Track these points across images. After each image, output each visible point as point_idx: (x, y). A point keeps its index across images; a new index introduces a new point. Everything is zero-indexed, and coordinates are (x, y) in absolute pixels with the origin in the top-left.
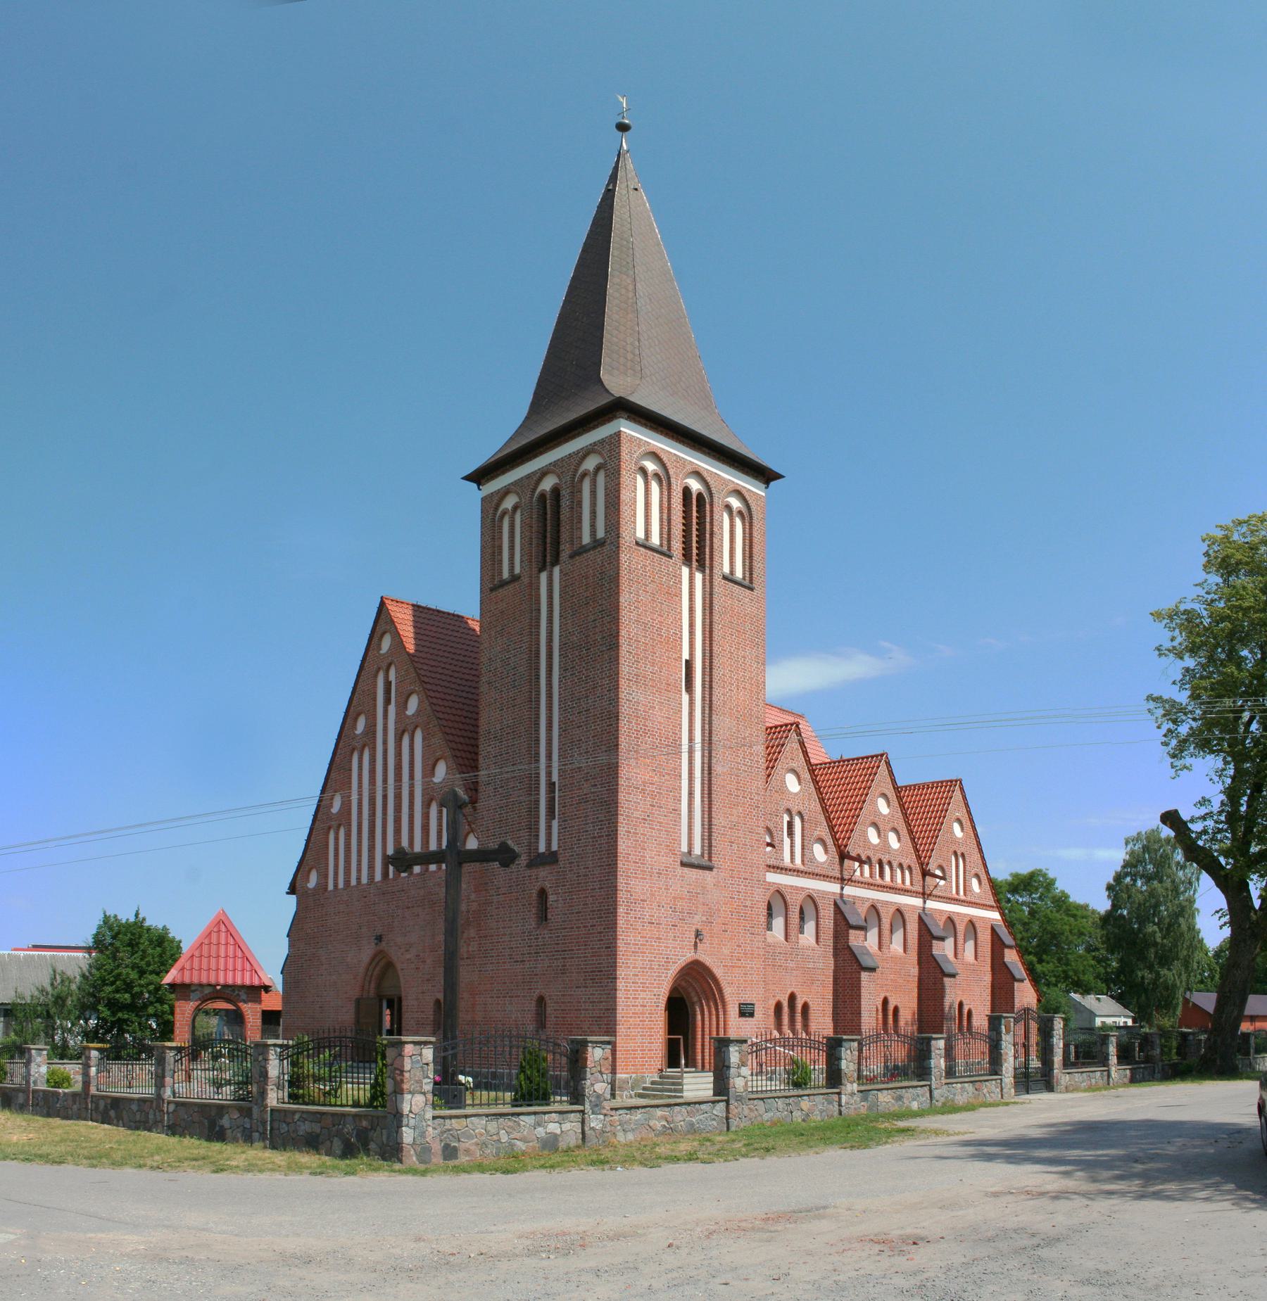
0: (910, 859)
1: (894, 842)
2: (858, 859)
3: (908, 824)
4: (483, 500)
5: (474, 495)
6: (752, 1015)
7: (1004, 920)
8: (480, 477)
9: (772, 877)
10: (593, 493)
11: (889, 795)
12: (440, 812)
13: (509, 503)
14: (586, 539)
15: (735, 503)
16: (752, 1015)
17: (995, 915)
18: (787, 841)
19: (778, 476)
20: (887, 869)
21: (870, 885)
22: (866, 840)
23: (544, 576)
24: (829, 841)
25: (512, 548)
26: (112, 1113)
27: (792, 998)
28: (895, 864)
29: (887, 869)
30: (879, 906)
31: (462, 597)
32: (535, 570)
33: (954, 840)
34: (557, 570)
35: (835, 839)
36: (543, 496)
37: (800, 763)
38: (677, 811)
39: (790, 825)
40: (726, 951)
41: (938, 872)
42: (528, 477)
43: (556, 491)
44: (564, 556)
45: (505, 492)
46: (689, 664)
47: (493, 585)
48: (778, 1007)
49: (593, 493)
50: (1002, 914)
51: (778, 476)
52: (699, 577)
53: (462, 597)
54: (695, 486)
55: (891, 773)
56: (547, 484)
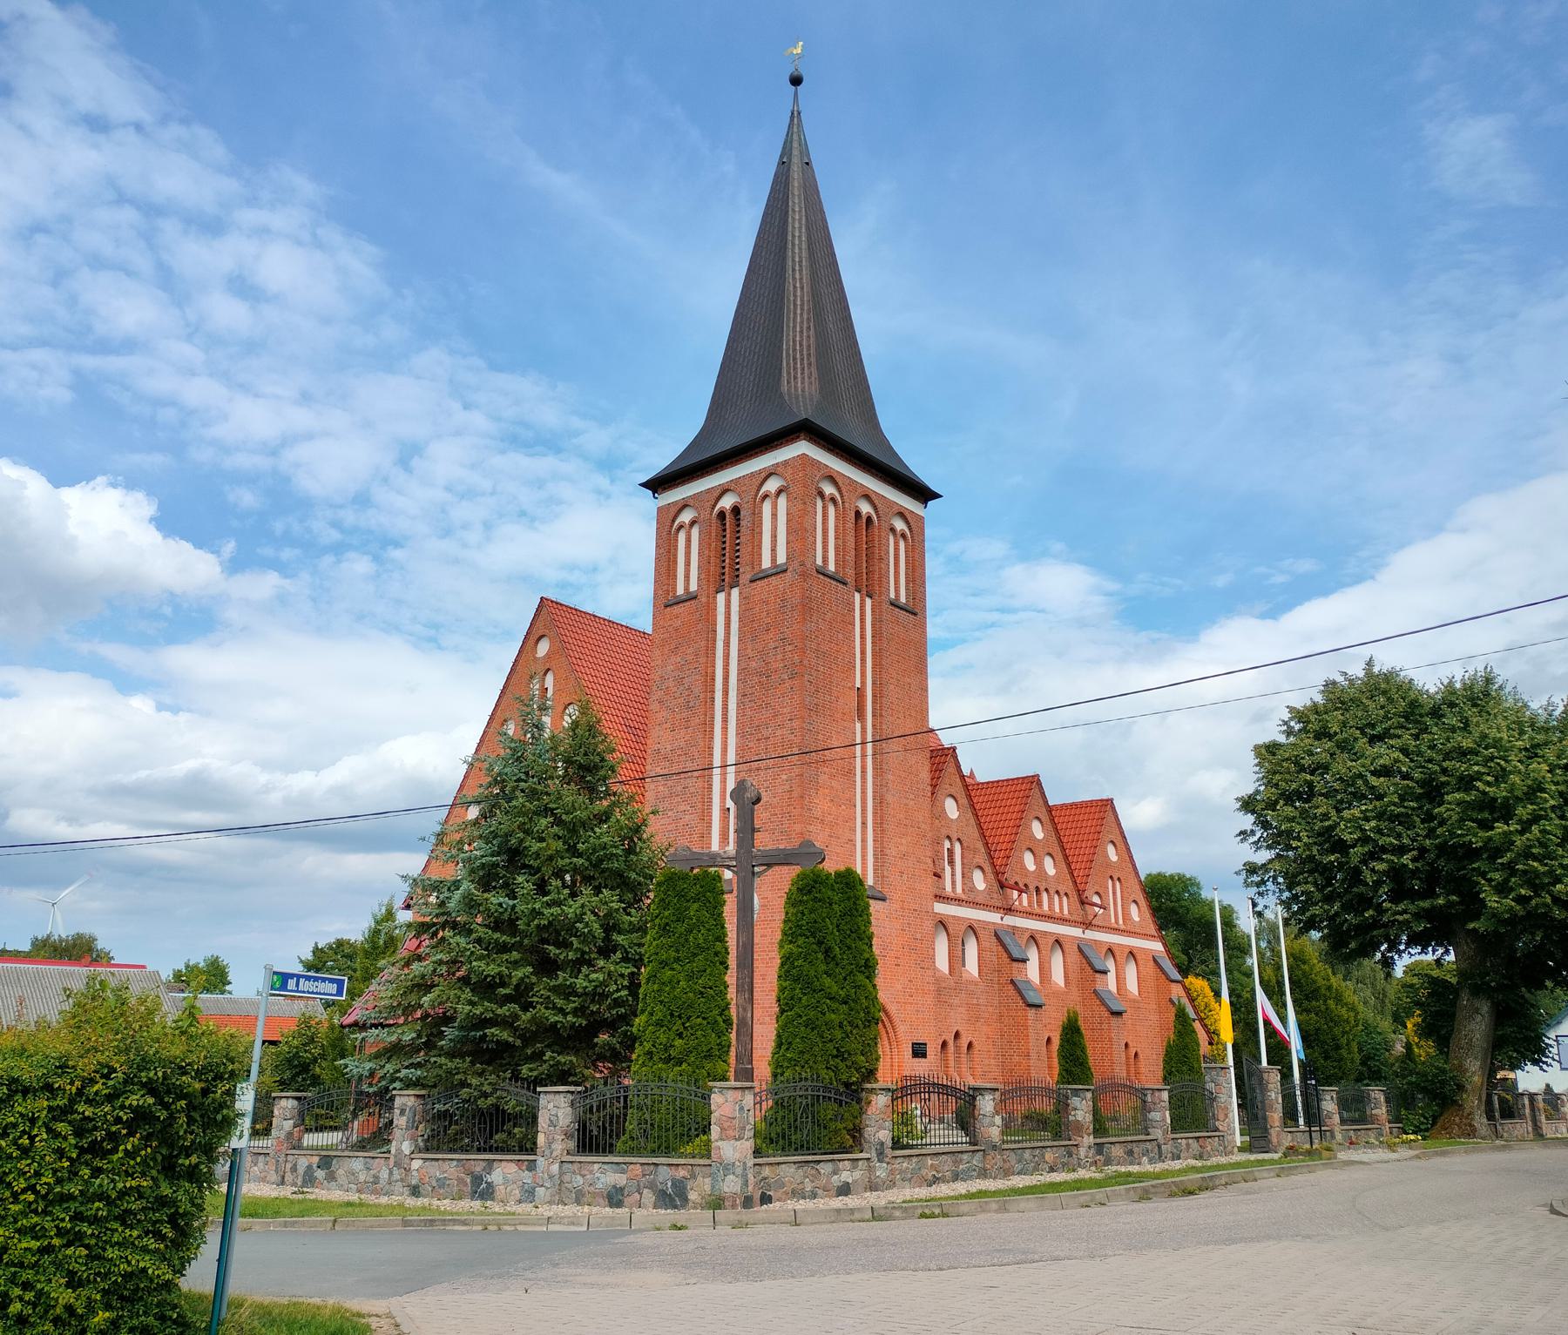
0: (1067, 886)
1: (1050, 867)
2: (1016, 886)
3: (1063, 849)
4: (659, 509)
5: (650, 504)
6: (924, 1056)
7: (1168, 951)
8: (657, 485)
9: (940, 908)
10: (774, 515)
11: (958, 796)
12: (825, 559)
13: (686, 517)
14: (766, 563)
15: (900, 525)
16: (924, 1056)
17: (1157, 946)
18: (948, 869)
19: (936, 496)
20: (1045, 895)
21: (1029, 914)
22: (1023, 867)
23: (721, 597)
24: (988, 868)
25: (688, 564)
26: (320, 1174)
27: (957, 1035)
28: (1052, 891)
29: (1045, 895)
30: (1037, 936)
31: (628, 599)
32: (712, 589)
33: (1108, 864)
34: (735, 592)
35: (993, 865)
36: (722, 515)
37: (958, 789)
38: (852, 841)
39: (951, 852)
40: (899, 987)
41: (1096, 899)
42: (708, 491)
43: (736, 510)
44: (745, 578)
45: (684, 506)
46: (861, 692)
47: (666, 600)
48: (944, 1044)
49: (774, 515)
50: (1165, 945)
51: (936, 496)
52: (868, 601)
53: (628, 599)
54: (865, 508)
55: (1043, 794)
56: (727, 502)
